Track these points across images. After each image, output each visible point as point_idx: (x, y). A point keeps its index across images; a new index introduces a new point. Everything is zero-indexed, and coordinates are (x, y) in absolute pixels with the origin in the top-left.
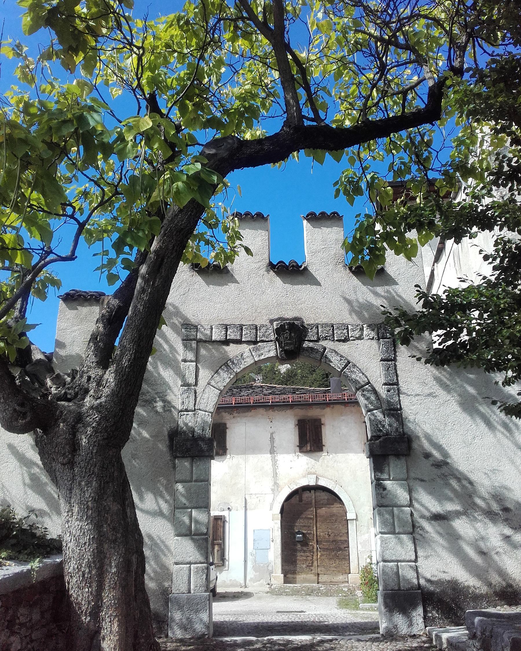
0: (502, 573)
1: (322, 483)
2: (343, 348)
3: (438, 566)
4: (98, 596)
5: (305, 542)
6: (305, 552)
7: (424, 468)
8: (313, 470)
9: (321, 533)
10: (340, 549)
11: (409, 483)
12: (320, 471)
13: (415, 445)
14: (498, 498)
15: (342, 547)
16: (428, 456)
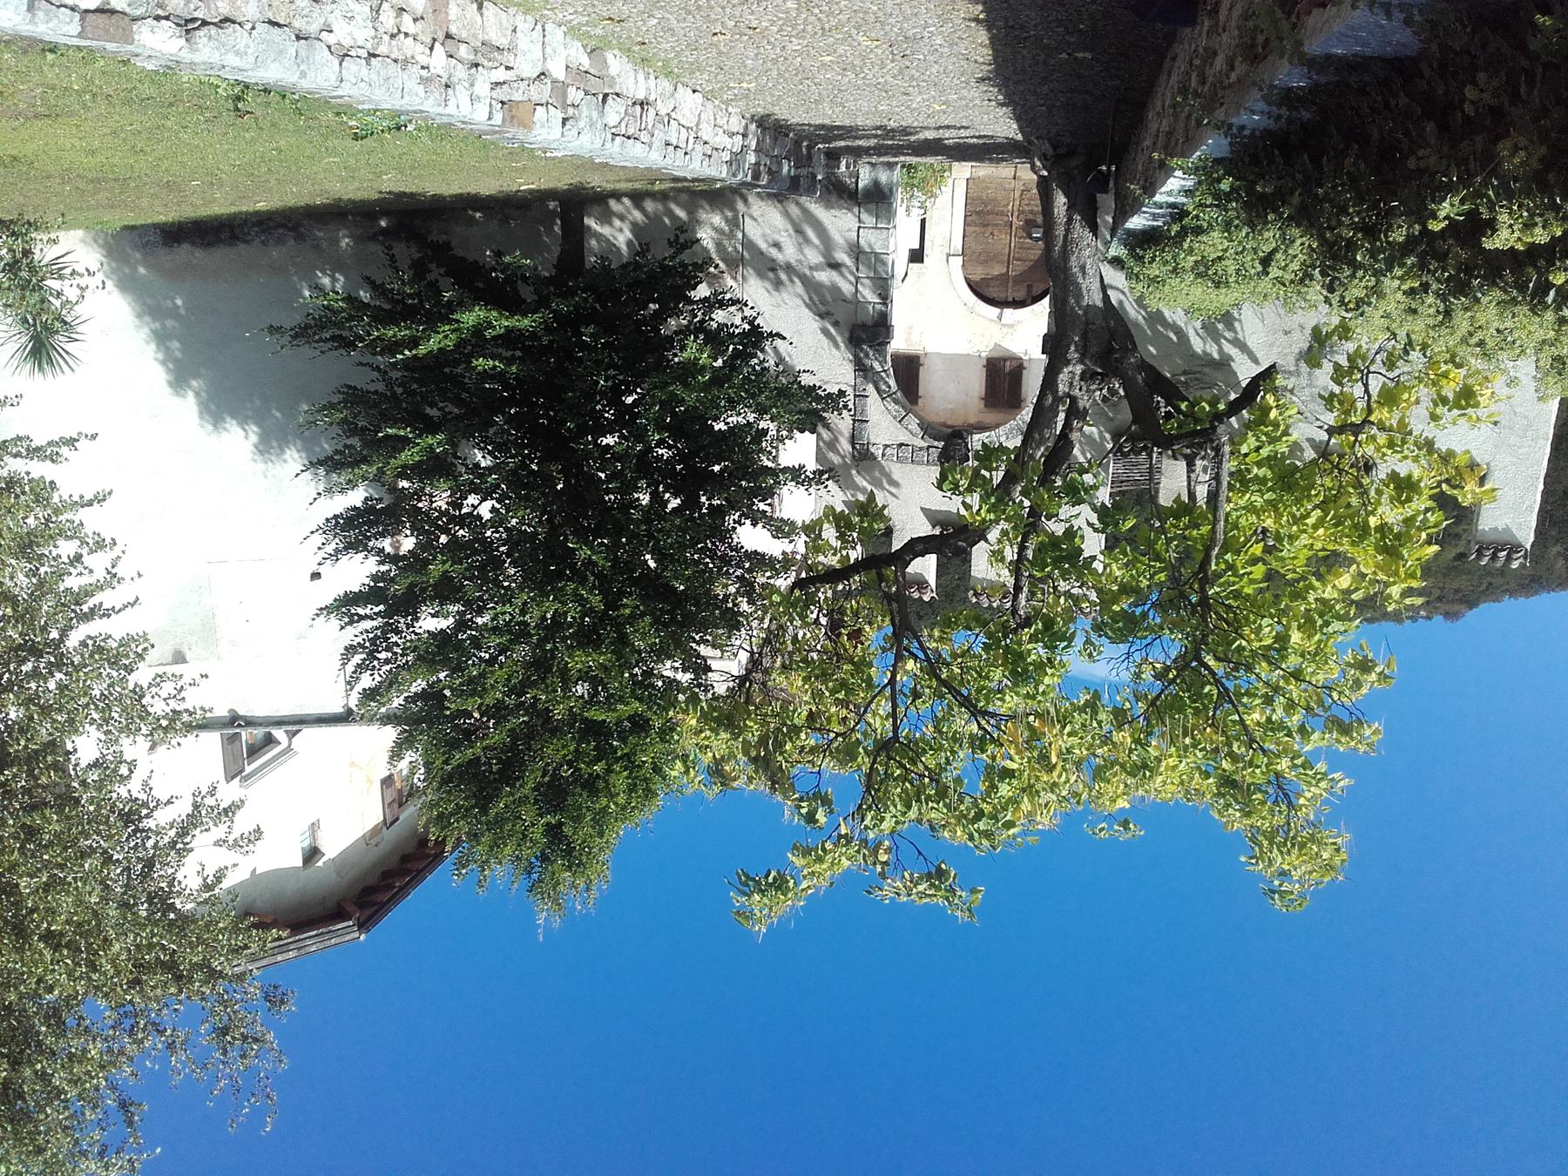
0: (786, 214)
1: (996, 311)
2: (904, 437)
3: (841, 223)
4: (1067, 231)
5: (1029, 225)
6: (1032, 212)
7: (841, 313)
8: (1005, 330)
9: (1004, 238)
10: (978, 213)
11: (856, 303)
12: (995, 327)
13: (847, 335)
14: (778, 284)
15: (974, 217)
16: (836, 324)
